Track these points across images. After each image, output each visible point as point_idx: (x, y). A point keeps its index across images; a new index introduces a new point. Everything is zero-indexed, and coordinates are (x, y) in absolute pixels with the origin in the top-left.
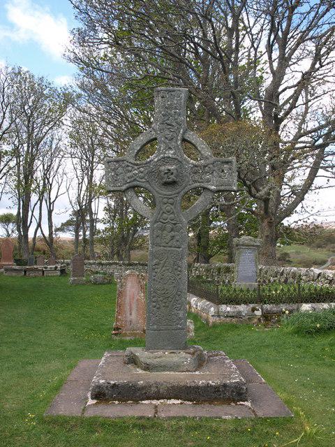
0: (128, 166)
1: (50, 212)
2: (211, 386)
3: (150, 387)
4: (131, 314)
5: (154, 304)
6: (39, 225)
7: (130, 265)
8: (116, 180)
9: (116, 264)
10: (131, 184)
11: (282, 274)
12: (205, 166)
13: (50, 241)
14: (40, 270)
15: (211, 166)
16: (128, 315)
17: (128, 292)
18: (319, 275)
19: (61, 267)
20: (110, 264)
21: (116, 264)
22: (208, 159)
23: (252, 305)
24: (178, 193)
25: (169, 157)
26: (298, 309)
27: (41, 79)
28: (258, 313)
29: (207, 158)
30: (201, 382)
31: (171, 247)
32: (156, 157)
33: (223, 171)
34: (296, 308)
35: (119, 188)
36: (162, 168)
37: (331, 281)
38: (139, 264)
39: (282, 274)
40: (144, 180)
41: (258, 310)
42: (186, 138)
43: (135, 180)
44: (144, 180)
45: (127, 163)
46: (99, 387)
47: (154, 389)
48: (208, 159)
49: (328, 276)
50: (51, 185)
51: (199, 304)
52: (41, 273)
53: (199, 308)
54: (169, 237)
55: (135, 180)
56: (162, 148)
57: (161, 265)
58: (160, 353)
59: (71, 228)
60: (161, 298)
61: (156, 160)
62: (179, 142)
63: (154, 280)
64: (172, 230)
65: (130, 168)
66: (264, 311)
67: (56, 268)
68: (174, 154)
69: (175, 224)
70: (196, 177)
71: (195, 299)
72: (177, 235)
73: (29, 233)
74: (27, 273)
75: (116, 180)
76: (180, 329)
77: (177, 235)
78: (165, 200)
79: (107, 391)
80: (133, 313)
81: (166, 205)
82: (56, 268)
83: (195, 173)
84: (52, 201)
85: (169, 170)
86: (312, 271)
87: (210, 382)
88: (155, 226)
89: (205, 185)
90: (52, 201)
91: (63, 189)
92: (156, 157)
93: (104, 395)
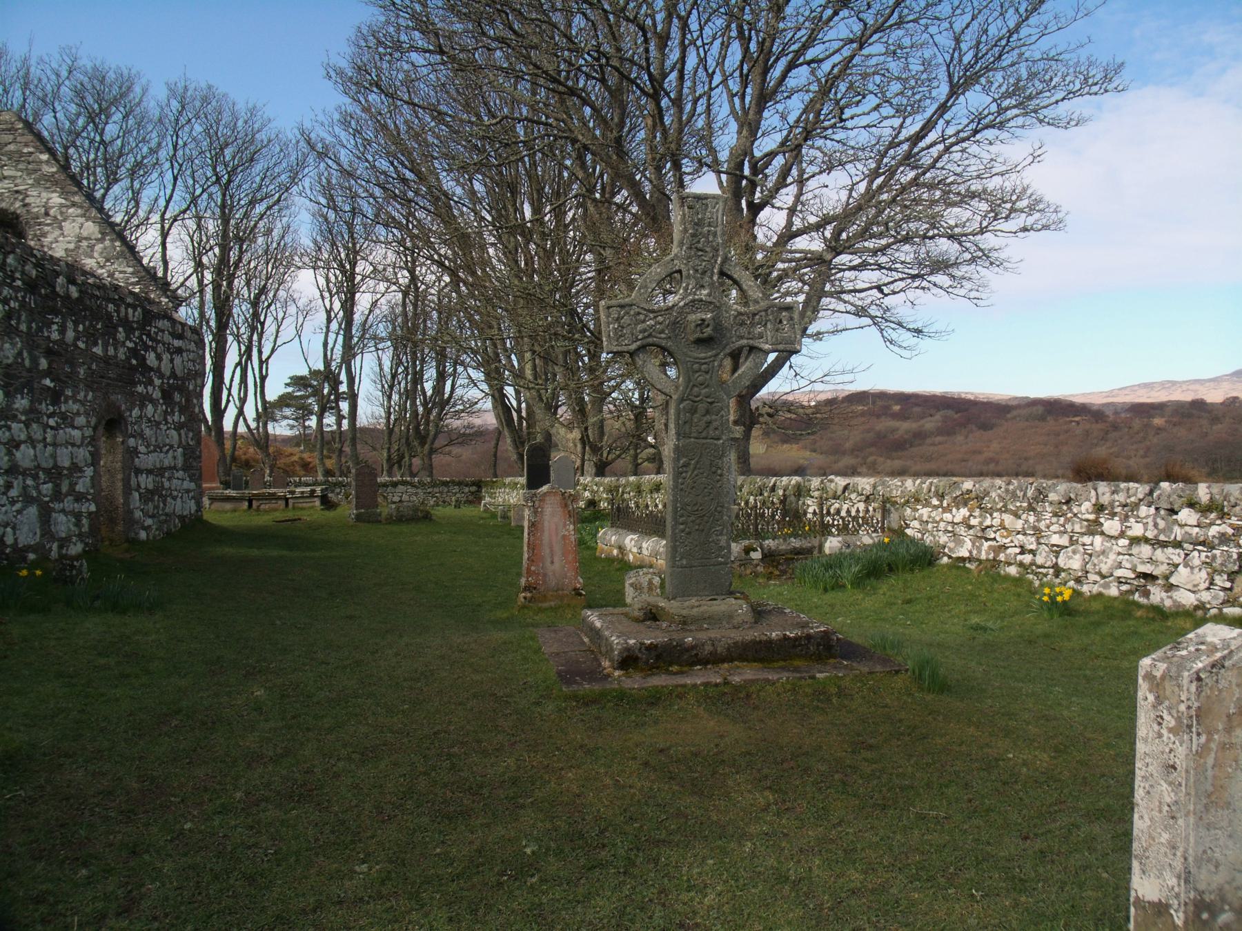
0: (639, 313)
1: (263, 379)
2: (789, 638)
3: (703, 645)
4: (552, 562)
5: (682, 527)
6: (241, 412)
7: (434, 484)
8: (621, 336)
9: (404, 483)
10: (645, 342)
11: (773, 489)
12: (754, 315)
13: (262, 441)
14: (279, 498)
15: (763, 313)
16: (548, 563)
17: (546, 524)
18: (846, 488)
19: (322, 490)
20: (395, 485)
21: (404, 483)
22: (758, 302)
23: (747, 542)
24: (716, 355)
25: (701, 300)
26: (821, 547)
27: (253, 111)
28: (756, 555)
29: (756, 302)
30: (774, 634)
31: (706, 438)
32: (682, 299)
33: (781, 322)
34: (816, 544)
35: (625, 348)
36: (692, 317)
37: (868, 497)
38: (453, 482)
39: (773, 489)
40: (663, 336)
41: (755, 550)
42: (725, 270)
43: (650, 335)
44: (663, 336)
45: (637, 310)
46: (628, 649)
47: (708, 648)
48: (758, 302)
49: (863, 489)
50: (263, 324)
51: (645, 545)
52: (282, 503)
53: (645, 552)
54: (702, 424)
55: (650, 335)
56: (690, 287)
57: (692, 467)
58: (694, 601)
59: (288, 412)
60: (692, 518)
61: (682, 304)
62: (715, 278)
63: (682, 490)
64: (707, 412)
65: (642, 317)
66: (766, 551)
67: (313, 491)
68: (709, 295)
69: (711, 403)
70: (743, 331)
71: (635, 537)
72: (716, 420)
73: (225, 422)
74: (255, 504)
75: (621, 336)
76: (721, 563)
77: (716, 420)
78: (696, 366)
79: (640, 655)
80: (556, 559)
81: (697, 375)
82: (313, 491)
83: (741, 325)
84: (264, 358)
85: (703, 320)
86: (831, 481)
87: (788, 633)
88: (681, 406)
89: (756, 343)
90: (264, 358)
91: (288, 331)
92: (682, 299)
93: (636, 659)
